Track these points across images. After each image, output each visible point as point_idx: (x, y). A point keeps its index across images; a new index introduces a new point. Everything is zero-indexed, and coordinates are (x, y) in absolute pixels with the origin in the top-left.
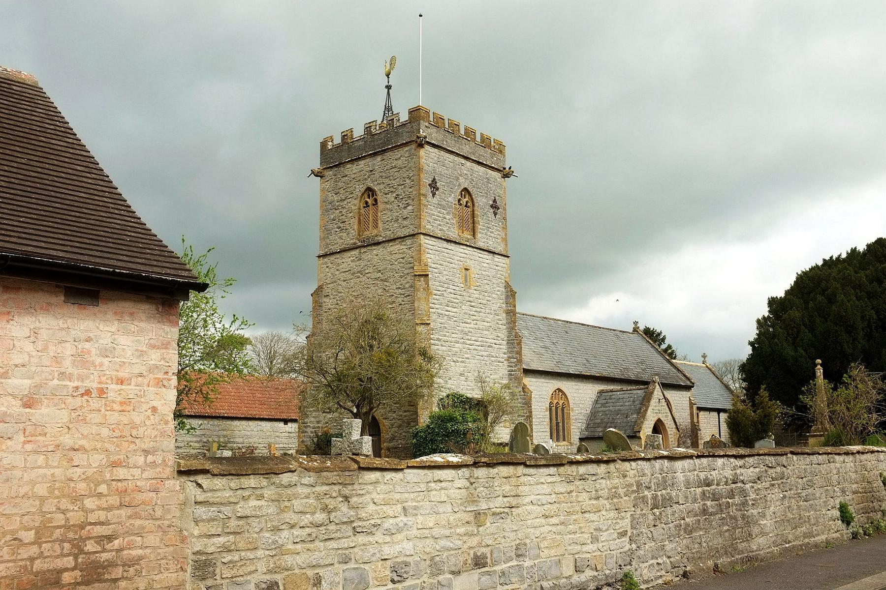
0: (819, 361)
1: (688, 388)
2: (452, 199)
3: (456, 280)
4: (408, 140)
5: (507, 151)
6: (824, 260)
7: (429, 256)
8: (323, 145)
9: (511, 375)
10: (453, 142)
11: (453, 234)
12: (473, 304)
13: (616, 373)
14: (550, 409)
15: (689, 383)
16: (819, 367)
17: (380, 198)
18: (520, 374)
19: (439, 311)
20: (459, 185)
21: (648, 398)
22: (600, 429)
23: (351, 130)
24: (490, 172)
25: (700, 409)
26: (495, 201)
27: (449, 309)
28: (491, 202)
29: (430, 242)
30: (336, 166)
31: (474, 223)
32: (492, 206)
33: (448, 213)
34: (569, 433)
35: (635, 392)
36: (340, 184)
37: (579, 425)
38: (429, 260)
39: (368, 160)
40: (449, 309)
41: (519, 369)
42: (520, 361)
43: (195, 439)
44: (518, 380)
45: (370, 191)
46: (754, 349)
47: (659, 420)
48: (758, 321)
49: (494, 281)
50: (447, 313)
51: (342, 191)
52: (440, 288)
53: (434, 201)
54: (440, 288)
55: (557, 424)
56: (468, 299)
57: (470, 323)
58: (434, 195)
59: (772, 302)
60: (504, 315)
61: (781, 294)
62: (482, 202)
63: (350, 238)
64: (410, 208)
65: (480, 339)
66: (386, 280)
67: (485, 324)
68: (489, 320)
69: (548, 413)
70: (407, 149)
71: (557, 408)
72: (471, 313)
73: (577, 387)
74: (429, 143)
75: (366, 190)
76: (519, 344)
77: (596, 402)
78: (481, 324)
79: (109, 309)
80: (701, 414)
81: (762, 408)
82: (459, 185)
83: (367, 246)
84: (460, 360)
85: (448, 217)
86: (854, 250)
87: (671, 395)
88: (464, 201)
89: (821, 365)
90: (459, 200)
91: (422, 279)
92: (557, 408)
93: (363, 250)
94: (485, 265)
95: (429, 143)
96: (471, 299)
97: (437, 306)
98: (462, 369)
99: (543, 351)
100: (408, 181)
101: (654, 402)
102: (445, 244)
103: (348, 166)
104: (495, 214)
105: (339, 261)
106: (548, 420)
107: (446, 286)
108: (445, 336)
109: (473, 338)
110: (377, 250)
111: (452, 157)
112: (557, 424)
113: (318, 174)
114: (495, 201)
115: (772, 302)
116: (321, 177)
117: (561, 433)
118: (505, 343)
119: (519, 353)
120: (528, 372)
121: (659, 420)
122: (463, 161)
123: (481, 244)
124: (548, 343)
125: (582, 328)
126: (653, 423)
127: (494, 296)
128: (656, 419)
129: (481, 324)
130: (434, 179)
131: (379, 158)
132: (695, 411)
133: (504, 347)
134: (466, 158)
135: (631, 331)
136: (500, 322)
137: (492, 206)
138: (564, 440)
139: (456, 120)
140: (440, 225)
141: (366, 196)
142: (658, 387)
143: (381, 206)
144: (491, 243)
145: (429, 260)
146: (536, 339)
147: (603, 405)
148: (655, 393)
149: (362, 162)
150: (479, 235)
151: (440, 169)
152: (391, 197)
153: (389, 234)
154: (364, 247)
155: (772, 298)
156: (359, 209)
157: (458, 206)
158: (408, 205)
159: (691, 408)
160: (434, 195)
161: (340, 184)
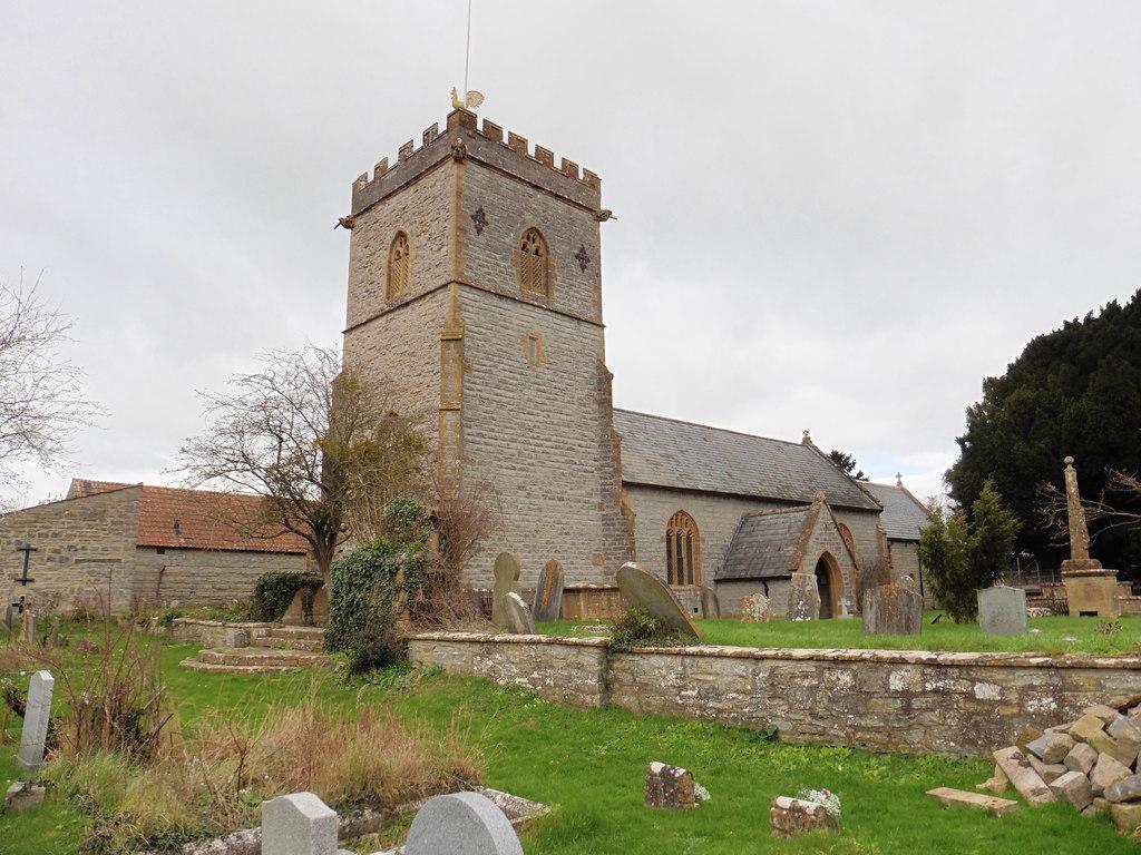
0: (1069, 459)
2: (512, 240)
3: (515, 352)
6: (1066, 323)
9: (604, 490)
10: (514, 163)
11: (512, 287)
12: (542, 388)
13: (771, 492)
14: (669, 541)
15: (876, 507)
16: (1070, 467)
18: (618, 489)
19: (484, 394)
20: (524, 223)
21: (810, 522)
22: (742, 567)
24: (576, 211)
25: (892, 540)
26: (582, 250)
28: (576, 252)
29: (471, 296)
31: (547, 276)
32: (577, 257)
34: (699, 574)
35: (792, 515)
37: (714, 561)
42: (618, 471)
43: (244, 580)
44: (615, 497)
45: (401, 234)
46: (964, 449)
47: (826, 554)
48: (970, 412)
49: (579, 358)
51: (372, 242)
52: (486, 362)
53: (481, 239)
54: (486, 362)
55: (680, 560)
56: (533, 380)
57: (537, 415)
58: (479, 231)
59: (990, 384)
60: (595, 406)
61: (1000, 372)
62: (560, 249)
63: (379, 304)
64: (444, 249)
66: (413, 354)
67: (563, 417)
69: (665, 544)
72: (539, 400)
73: (710, 509)
76: (617, 446)
78: (556, 418)
80: (895, 548)
81: (988, 523)
82: (524, 223)
83: (395, 309)
84: (519, 466)
85: (503, 264)
86: (1113, 307)
88: (532, 247)
89: (1073, 465)
91: (452, 345)
94: (563, 335)
97: (479, 387)
98: (521, 480)
99: (662, 460)
101: (818, 529)
102: (496, 301)
103: (380, 207)
105: (364, 335)
106: (664, 554)
107: (496, 359)
108: (493, 430)
109: (542, 436)
110: (405, 314)
111: (511, 183)
112: (680, 560)
113: (347, 224)
114: (582, 250)
115: (990, 384)
117: (686, 573)
118: (596, 445)
119: (617, 459)
120: (628, 486)
121: (826, 554)
122: (531, 191)
123: (559, 307)
124: (672, 450)
125: (728, 435)
128: (821, 552)
129: (556, 418)
130: (481, 210)
132: (885, 543)
133: (594, 451)
134: (536, 187)
135: (800, 442)
136: (588, 416)
137: (577, 257)
138: (691, 582)
139: (521, 134)
140: (489, 274)
141: (398, 243)
143: (412, 253)
144: (575, 305)
146: (656, 445)
148: (821, 515)
150: (556, 294)
151: (490, 197)
152: (423, 239)
154: (391, 311)
155: (990, 379)
157: (520, 252)
158: (442, 245)
159: (879, 539)
160: (479, 231)
161: (371, 234)
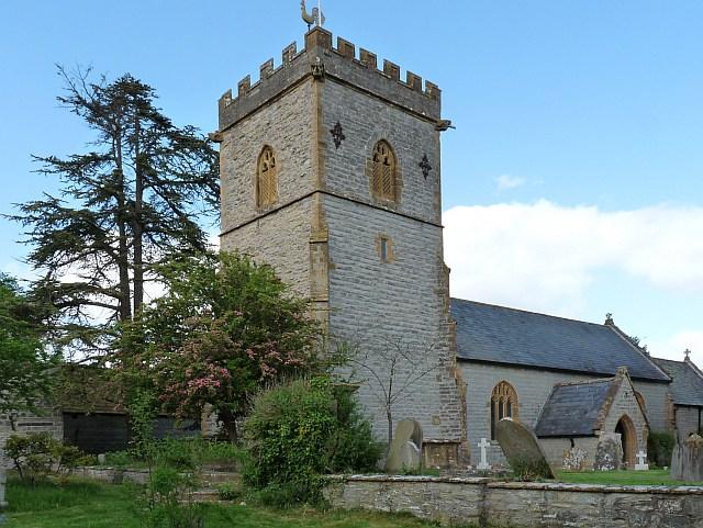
1: (667, 382)
2: (365, 151)
4: (304, 74)
5: (443, 96)
7: (329, 220)
8: (221, 102)
11: (367, 195)
15: (667, 377)
17: (279, 156)
20: (376, 135)
21: (613, 391)
23: (248, 78)
27: (358, 286)
29: (332, 204)
30: (232, 126)
32: (421, 165)
33: (359, 169)
36: (239, 148)
38: (331, 226)
39: (264, 111)
40: (358, 286)
41: (452, 358)
47: (625, 416)
50: (356, 291)
58: (338, 144)
62: (406, 159)
63: (251, 213)
64: (307, 162)
65: (402, 323)
67: (409, 305)
68: (415, 301)
70: (303, 87)
71: (501, 404)
74: (330, 77)
75: (263, 149)
77: (551, 397)
79: (484, 367)
87: (642, 388)
90: (375, 157)
92: (501, 404)
93: (261, 221)
95: (330, 77)
96: (391, 276)
97: (342, 282)
100: (305, 128)
101: (620, 396)
103: (246, 123)
104: (426, 175)
114: (425, 158)
116: (220, 142)
122: (381, 105)
126: (617, 419)
127: (422, 273)
128: (621, 415)
130: (338, 125)
131: (275, 106)
142: (626, 379)
145: (331, 226)
147: (559, 400)
149: (258, 115)
152: (287, 153)
153: (287, 199)
156: (258, 174)
160: (338, 144)
161: (239, 148)
